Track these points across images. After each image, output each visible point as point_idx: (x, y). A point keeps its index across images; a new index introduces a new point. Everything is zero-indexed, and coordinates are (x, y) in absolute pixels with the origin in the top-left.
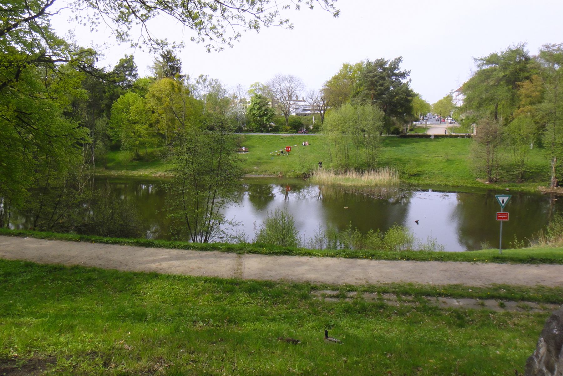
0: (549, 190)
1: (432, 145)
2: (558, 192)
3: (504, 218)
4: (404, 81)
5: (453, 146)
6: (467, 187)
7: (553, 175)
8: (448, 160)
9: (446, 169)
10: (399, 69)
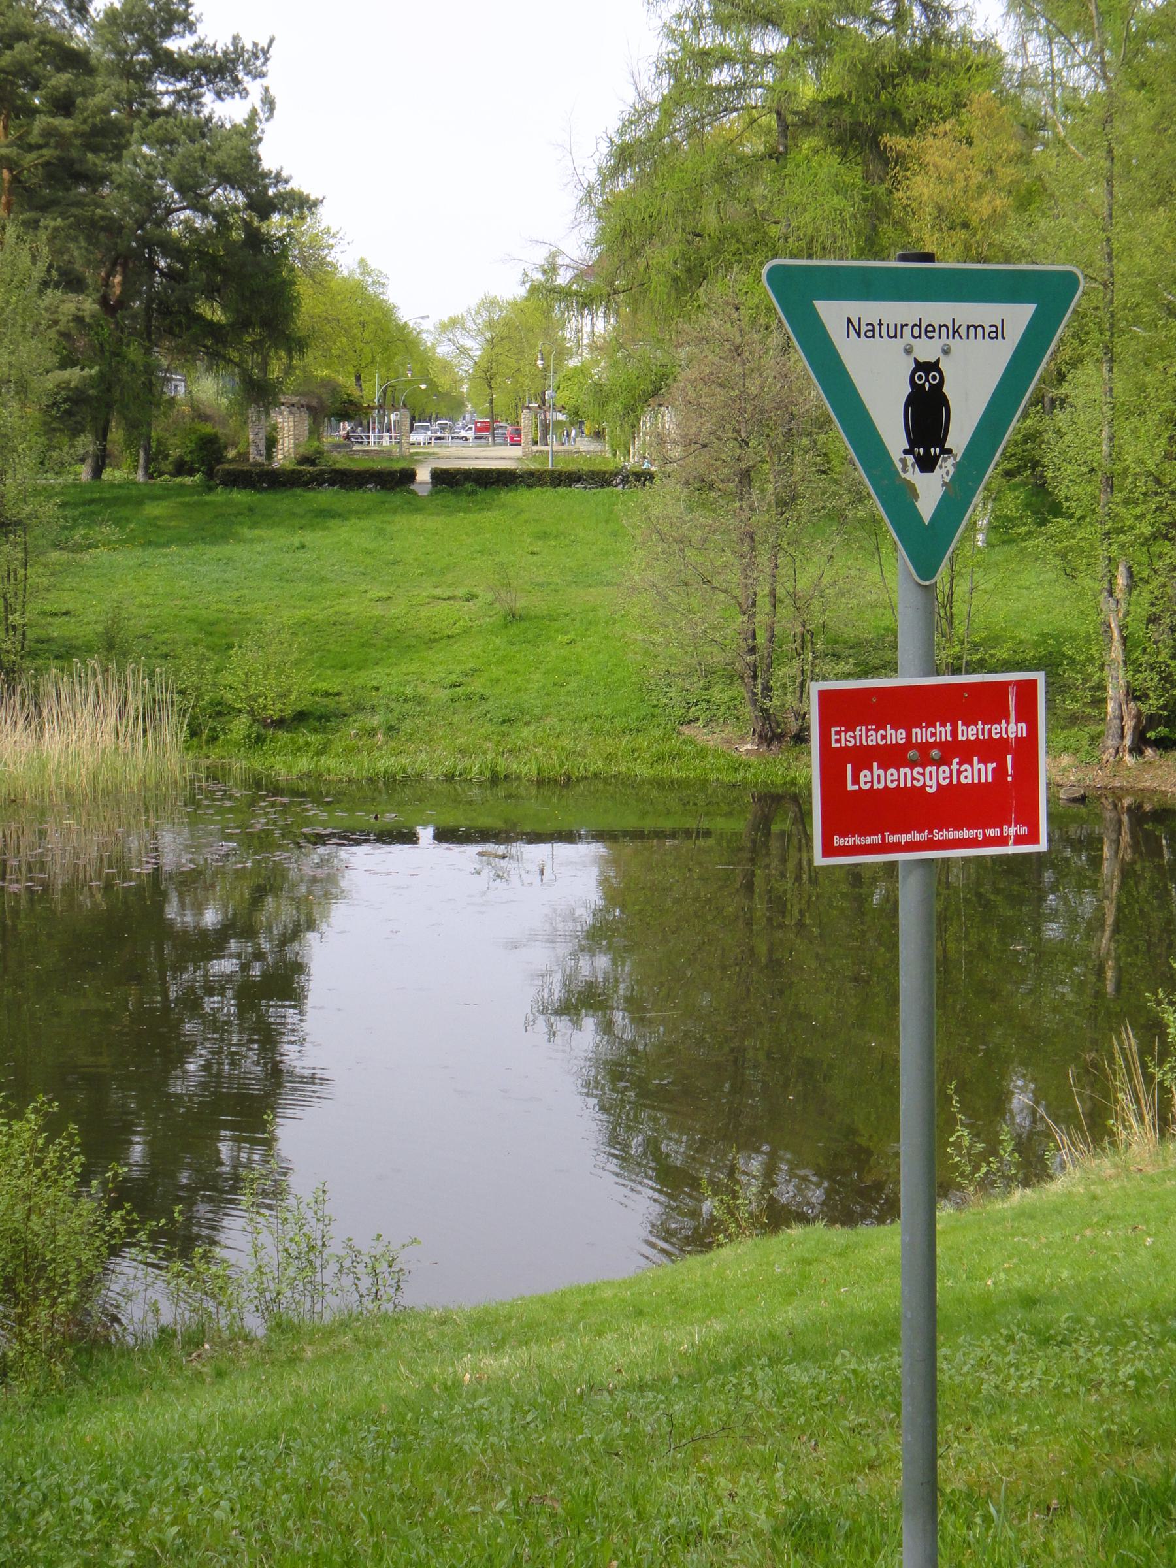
0: (1096, 777)
1: (421, 534)
2: (1148, 781)
3: (957, 807)
4: (228, 111)
5: (544, 536)
6: (628, 782)
7: (1116, 683)
8: (513, 617)
9: (497, 672)
10: (191, 27)
